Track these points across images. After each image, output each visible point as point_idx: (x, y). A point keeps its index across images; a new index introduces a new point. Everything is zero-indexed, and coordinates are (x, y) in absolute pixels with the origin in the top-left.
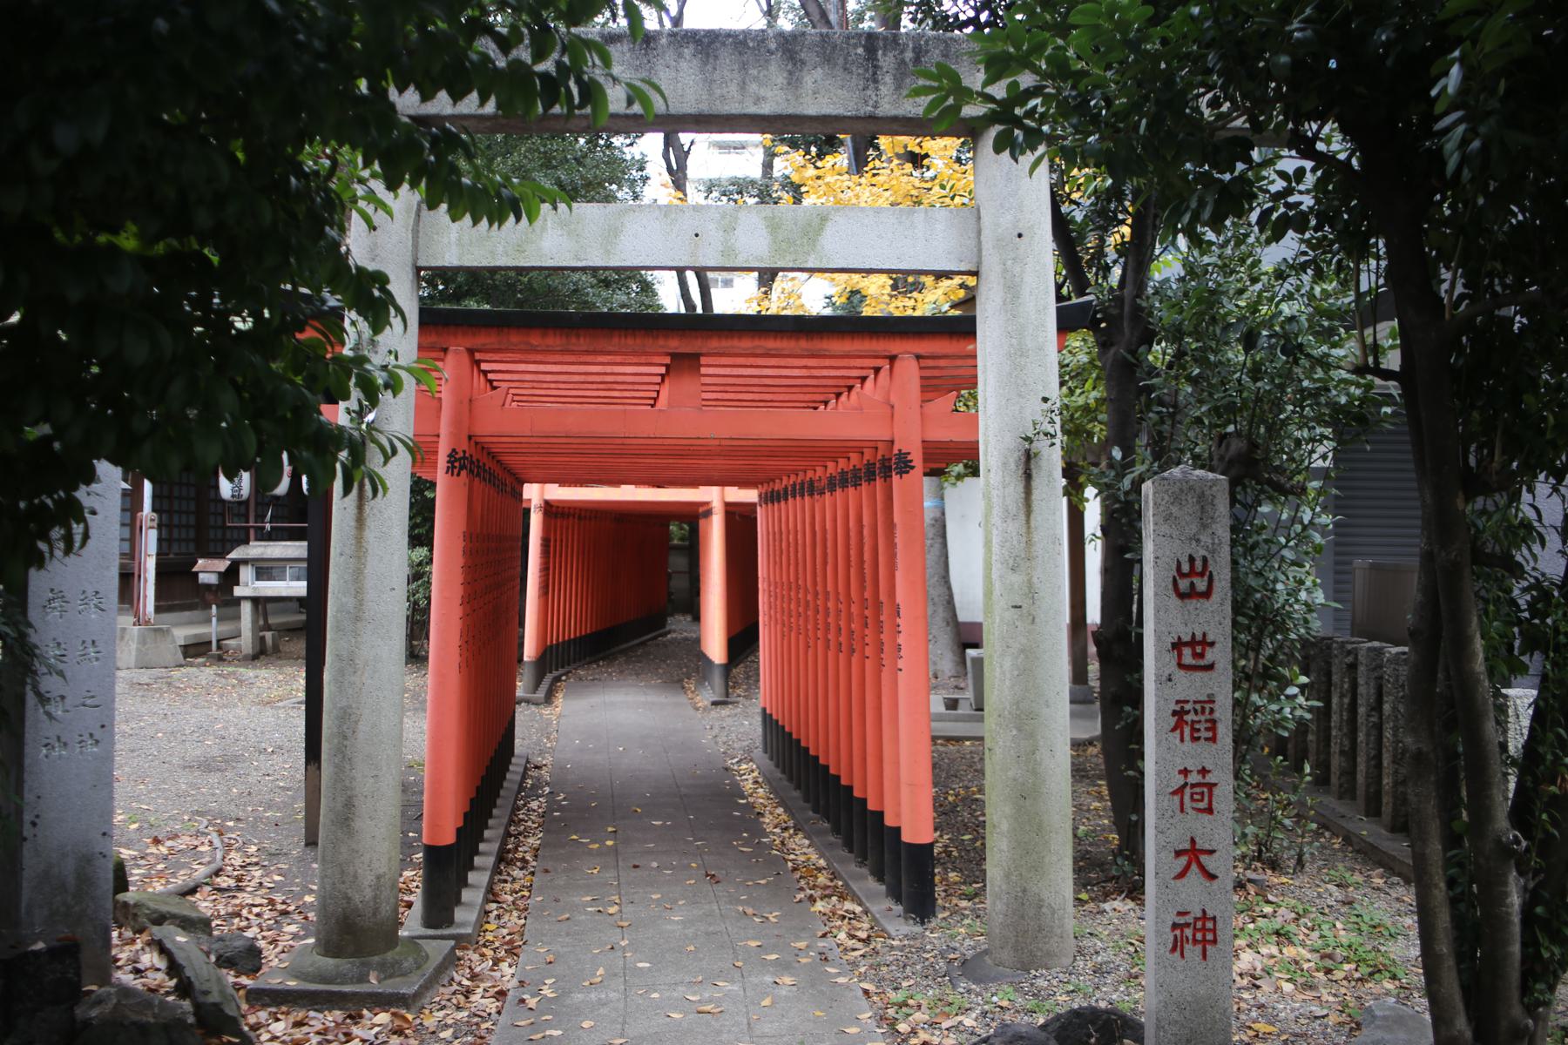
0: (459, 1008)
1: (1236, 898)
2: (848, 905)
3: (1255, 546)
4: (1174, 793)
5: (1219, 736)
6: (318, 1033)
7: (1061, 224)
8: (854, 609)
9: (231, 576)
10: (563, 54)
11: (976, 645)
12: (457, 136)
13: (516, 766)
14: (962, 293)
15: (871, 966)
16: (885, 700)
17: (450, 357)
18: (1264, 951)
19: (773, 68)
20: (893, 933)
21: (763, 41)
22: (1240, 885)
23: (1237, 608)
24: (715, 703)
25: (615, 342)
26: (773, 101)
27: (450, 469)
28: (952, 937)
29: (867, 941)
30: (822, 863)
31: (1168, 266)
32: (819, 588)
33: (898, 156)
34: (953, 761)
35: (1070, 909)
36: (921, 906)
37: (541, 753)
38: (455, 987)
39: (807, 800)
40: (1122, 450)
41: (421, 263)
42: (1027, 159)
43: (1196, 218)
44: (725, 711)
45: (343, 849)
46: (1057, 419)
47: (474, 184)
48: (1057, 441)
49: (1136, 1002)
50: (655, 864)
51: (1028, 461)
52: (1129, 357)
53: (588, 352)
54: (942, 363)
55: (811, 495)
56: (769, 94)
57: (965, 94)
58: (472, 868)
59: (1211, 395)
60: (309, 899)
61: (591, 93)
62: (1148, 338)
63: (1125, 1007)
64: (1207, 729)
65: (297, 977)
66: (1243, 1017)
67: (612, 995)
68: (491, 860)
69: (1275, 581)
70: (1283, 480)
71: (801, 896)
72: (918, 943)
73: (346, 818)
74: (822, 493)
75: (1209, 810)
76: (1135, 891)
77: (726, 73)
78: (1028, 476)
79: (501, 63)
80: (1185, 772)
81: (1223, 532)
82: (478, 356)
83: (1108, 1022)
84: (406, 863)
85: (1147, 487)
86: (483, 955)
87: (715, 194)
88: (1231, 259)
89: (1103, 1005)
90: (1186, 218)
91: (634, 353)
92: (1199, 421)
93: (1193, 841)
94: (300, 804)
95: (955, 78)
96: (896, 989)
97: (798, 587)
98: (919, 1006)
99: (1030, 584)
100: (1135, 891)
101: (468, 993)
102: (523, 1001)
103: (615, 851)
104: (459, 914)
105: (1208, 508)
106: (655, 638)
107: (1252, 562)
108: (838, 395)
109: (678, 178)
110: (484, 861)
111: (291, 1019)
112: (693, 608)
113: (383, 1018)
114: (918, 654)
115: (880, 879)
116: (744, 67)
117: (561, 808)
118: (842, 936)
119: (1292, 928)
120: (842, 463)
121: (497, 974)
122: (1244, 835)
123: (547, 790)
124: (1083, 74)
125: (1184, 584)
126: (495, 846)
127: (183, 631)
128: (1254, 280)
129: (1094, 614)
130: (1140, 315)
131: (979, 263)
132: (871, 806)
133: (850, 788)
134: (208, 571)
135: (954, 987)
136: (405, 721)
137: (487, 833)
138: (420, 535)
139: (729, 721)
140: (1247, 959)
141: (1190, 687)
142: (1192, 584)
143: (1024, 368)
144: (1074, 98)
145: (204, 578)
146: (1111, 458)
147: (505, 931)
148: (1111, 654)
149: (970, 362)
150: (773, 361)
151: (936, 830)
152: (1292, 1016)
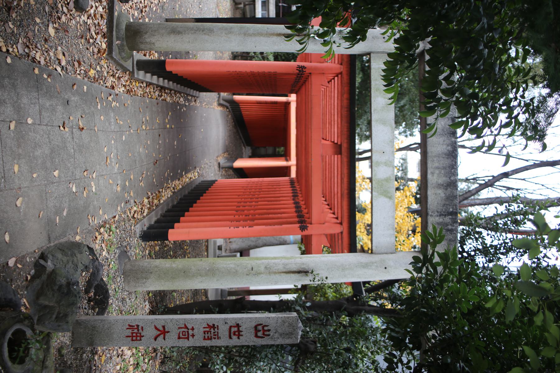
0: (108, 73)
1: (150, 349)
2: (146, 211)
3: (276, 354)
4: (185, 325)
5: (206, 341)
6: (98, 23)
7: (391, 283)
8: (252, 211)
10: (444, 100)
11: (241, 256)
12: (414, 63)
13: (195, 93)
14: (366, 249)
15: (124, 219)
16: (219, 223)
17: (339, 66)
18: (131, 359)
19: (444, 179)
20: (136, 227)
21: (454, 175)
22: (155, 350)
23: (254, 348)
24: (219, 164)
25: (345, 125)
26: (432, 179)
27: (299, 67)
28: (135, 248)
29: (133, 217)
30: (162, 201)
31: (377, 322)
32: (259, 199)
33: (415, 225)
34: (199, 248)
35: (146, 289)
36: (146, 236)
37: (200, 102)
38: (115, 71)
39: (184, 196)
40: (310, 306)
41: (372, 55)
42: (411, 268)
43: (392, 330)
44: (216, 167)
45: (163, 31)
46: (320, 283)
47: (397, 70)
48: (312, 283)
49: (112, 313)
50: (160, 142)
51: (304, 272)
52: (343, 308)
53: (341, 115)
54: (340, 241)
55: (293, 196)
56: (435, 177)
57: (434, 246)
58: (159, 77)
59: (330, 338)
60: (147, 20)
61: (431, 110)
62: (350, 315)
63: (110, 309)
64: (208, 337)
65: (118, 15)
66: (107, 351)
67: (113, 127)
68: (161, 84)
69: (264, 362)
70: (300, 364)
71: (150, 194)
72: (133, 235)
73: (174, 32)
74: (293, 200)
75: (179, 338)
76: (152, 312)
77: (442, 162)
78: (299, 272)
79: (441, 77)
80: (193, 329)
81: (279, 341)
82: (340, 76)
83: (104, 303)
84: (160, 53)
85: (295, 314)
86: (127, 81)
87: (402, 161)
88: (379, 344)
89: (111, 301)
90: (392, 327)
91: (341, 131)
92: (321, 333)
93: (168, 332)
94: (181, 17)
95: (439, 242)
96: (116, 227)
97: (260, 192)
98: (110, 236)
99: (260, 273)
100: (152, 312)
101: (113, 76)
102: (110, 95)
103: (165, 128)
104: (142, 73)
105: (287, 336)
106: (243, 142)
107: (271, 354)
108: (328, 205)
109: (408, 148)
110: (161, 82)
111: (103, 14)
112: (254, 155)
113: (104, 46)
114: (239, 234)
115: (156, 222)
116: (444, 168)
117: (180, 109)
118: (135, 208)
119: (140, 369)
120: (304, 207)
121: (120, 86)
122: (173, 352)
123: (187, 104)
124: (442, 288)
125: (260, 328)
126: (166, 86)
128: (372, 353)
129: (253, 298)
130: (358, 312)
131: (375, 254)
132: (182, 218)
133: (188, 211)
135: (117, 248)
136: (211, 53)
137: (171, 83)
138: (278, 57)
139: (213, 169)
140: (128, 353)
141: (223, 330)
142: (260, 331)
143: (337, 270)
144: (433, 285)
146: (307, 302)
147: (136, 89)
148: (238, 302)
149: (340, 251)
150: (339, 181)
151: (174, 242)
152: (108, 369)
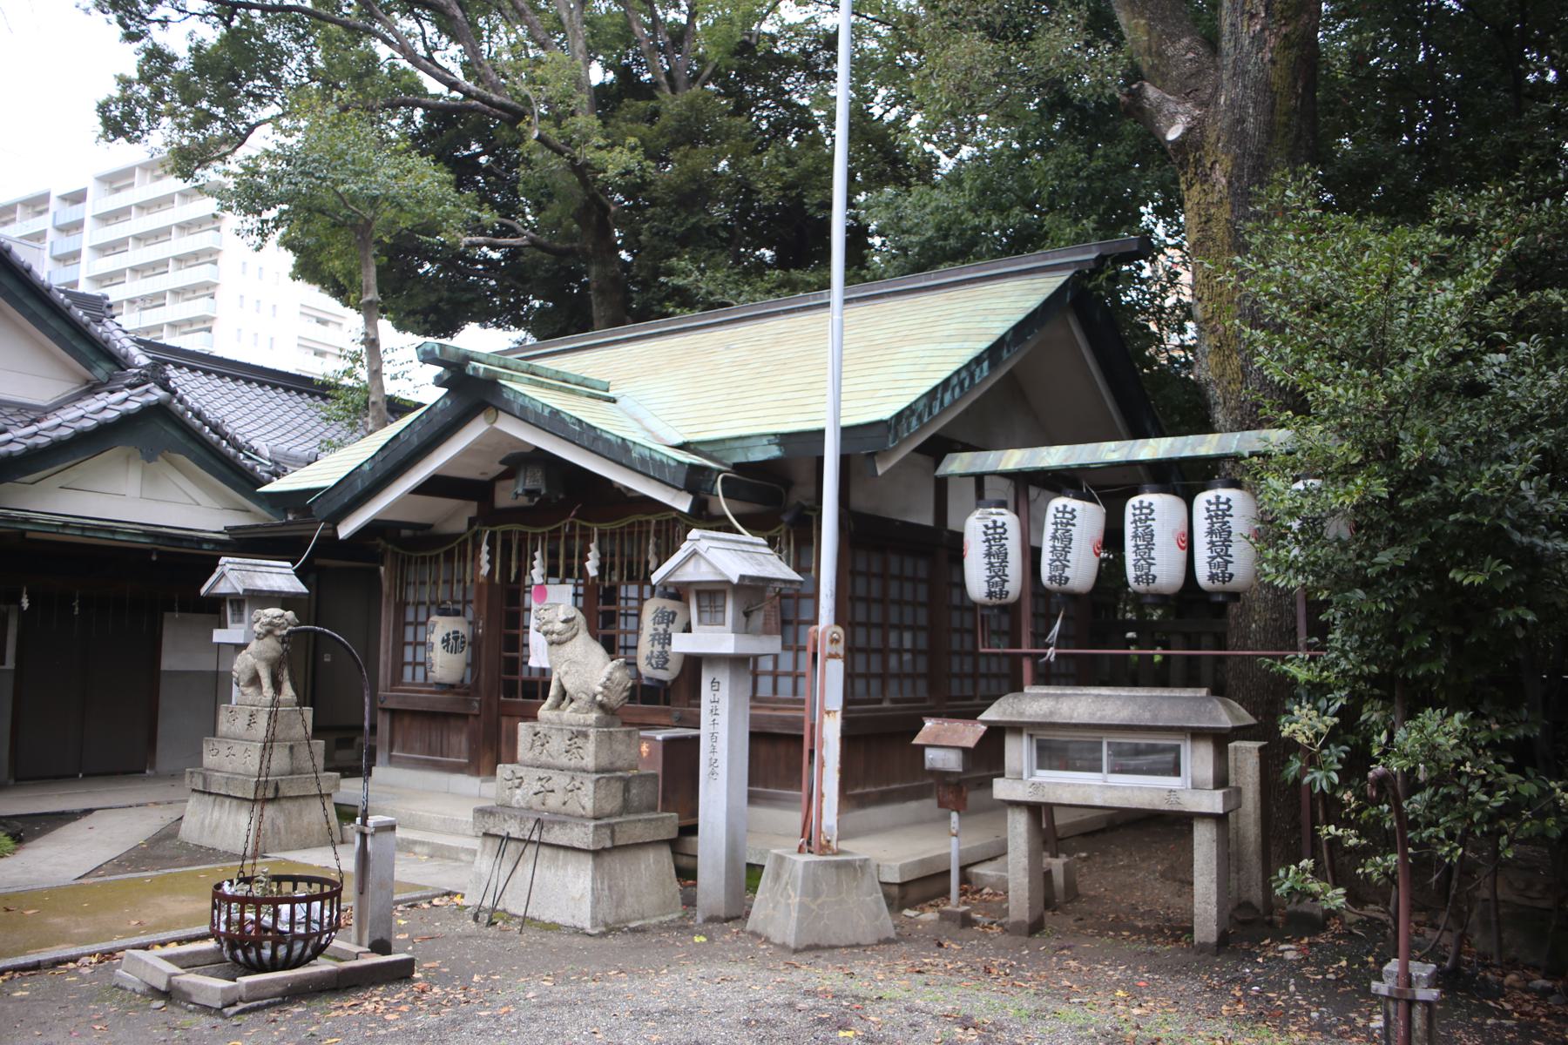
9: (987, 756)
127: (899, 845)
134: (944, 742)
145: (936, 758)
